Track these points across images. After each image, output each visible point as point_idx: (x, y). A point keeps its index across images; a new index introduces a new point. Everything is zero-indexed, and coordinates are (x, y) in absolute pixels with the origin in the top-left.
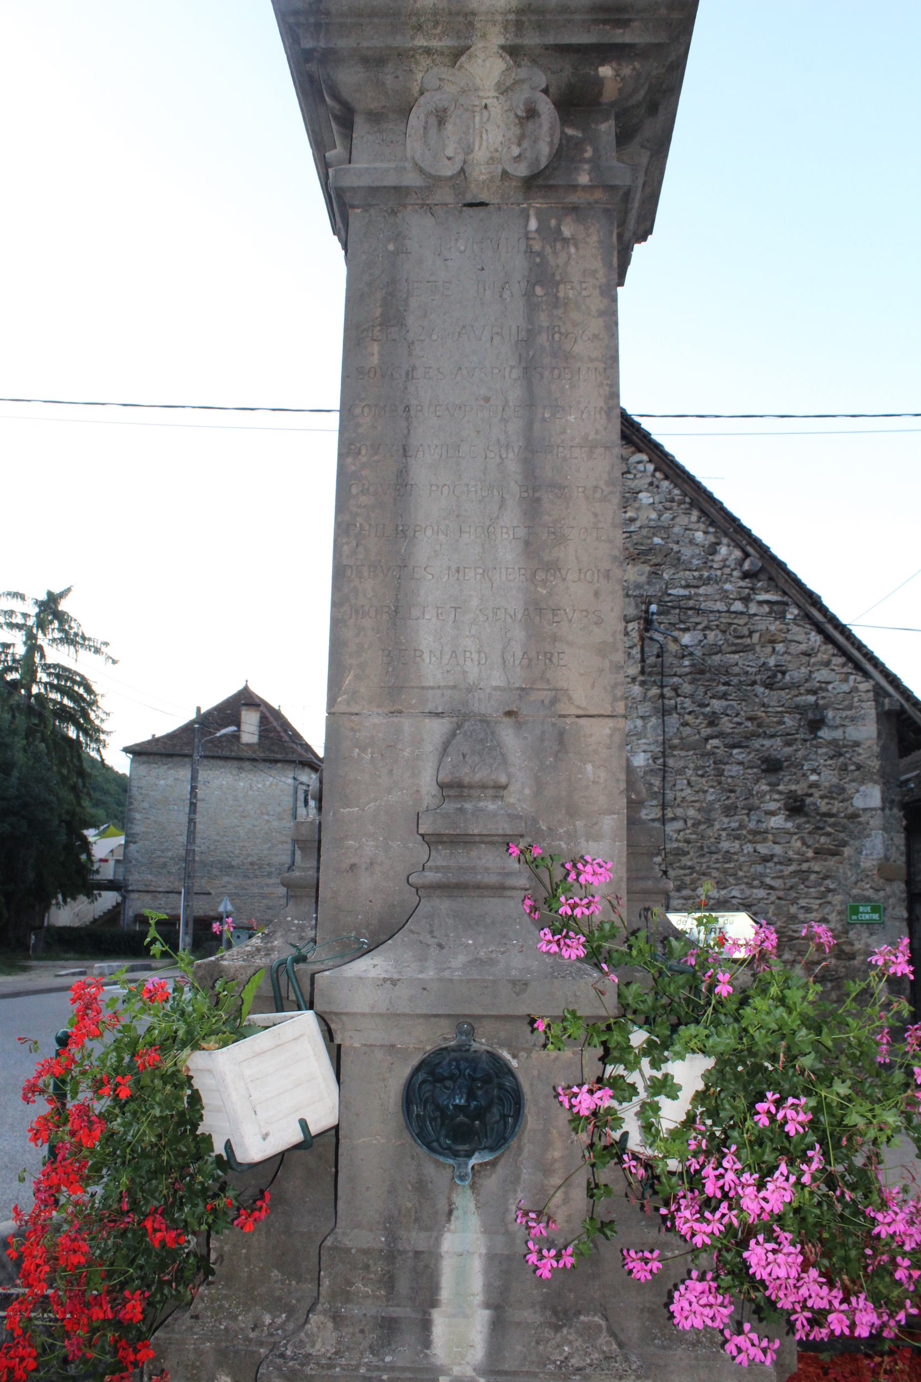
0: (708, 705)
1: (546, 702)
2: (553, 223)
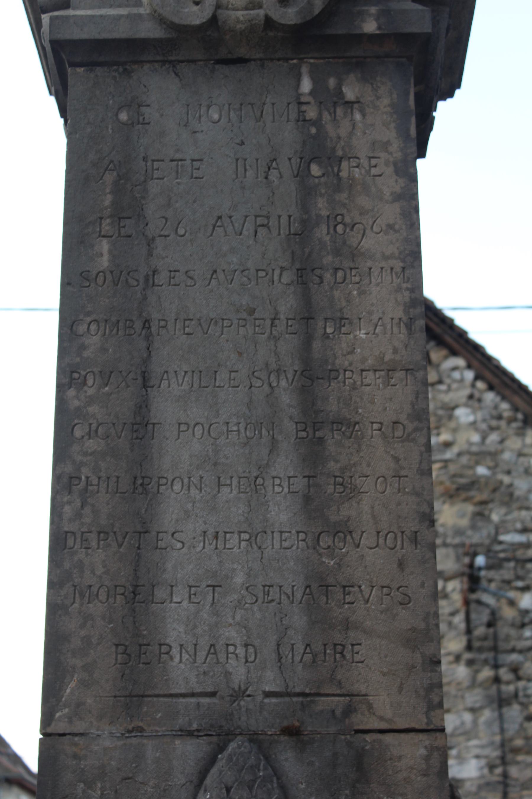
1: (338, 713)
2: (332, 82)
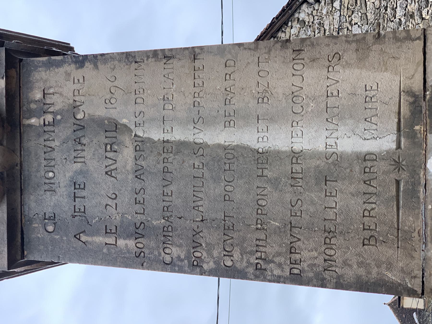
0: (400, 19)
